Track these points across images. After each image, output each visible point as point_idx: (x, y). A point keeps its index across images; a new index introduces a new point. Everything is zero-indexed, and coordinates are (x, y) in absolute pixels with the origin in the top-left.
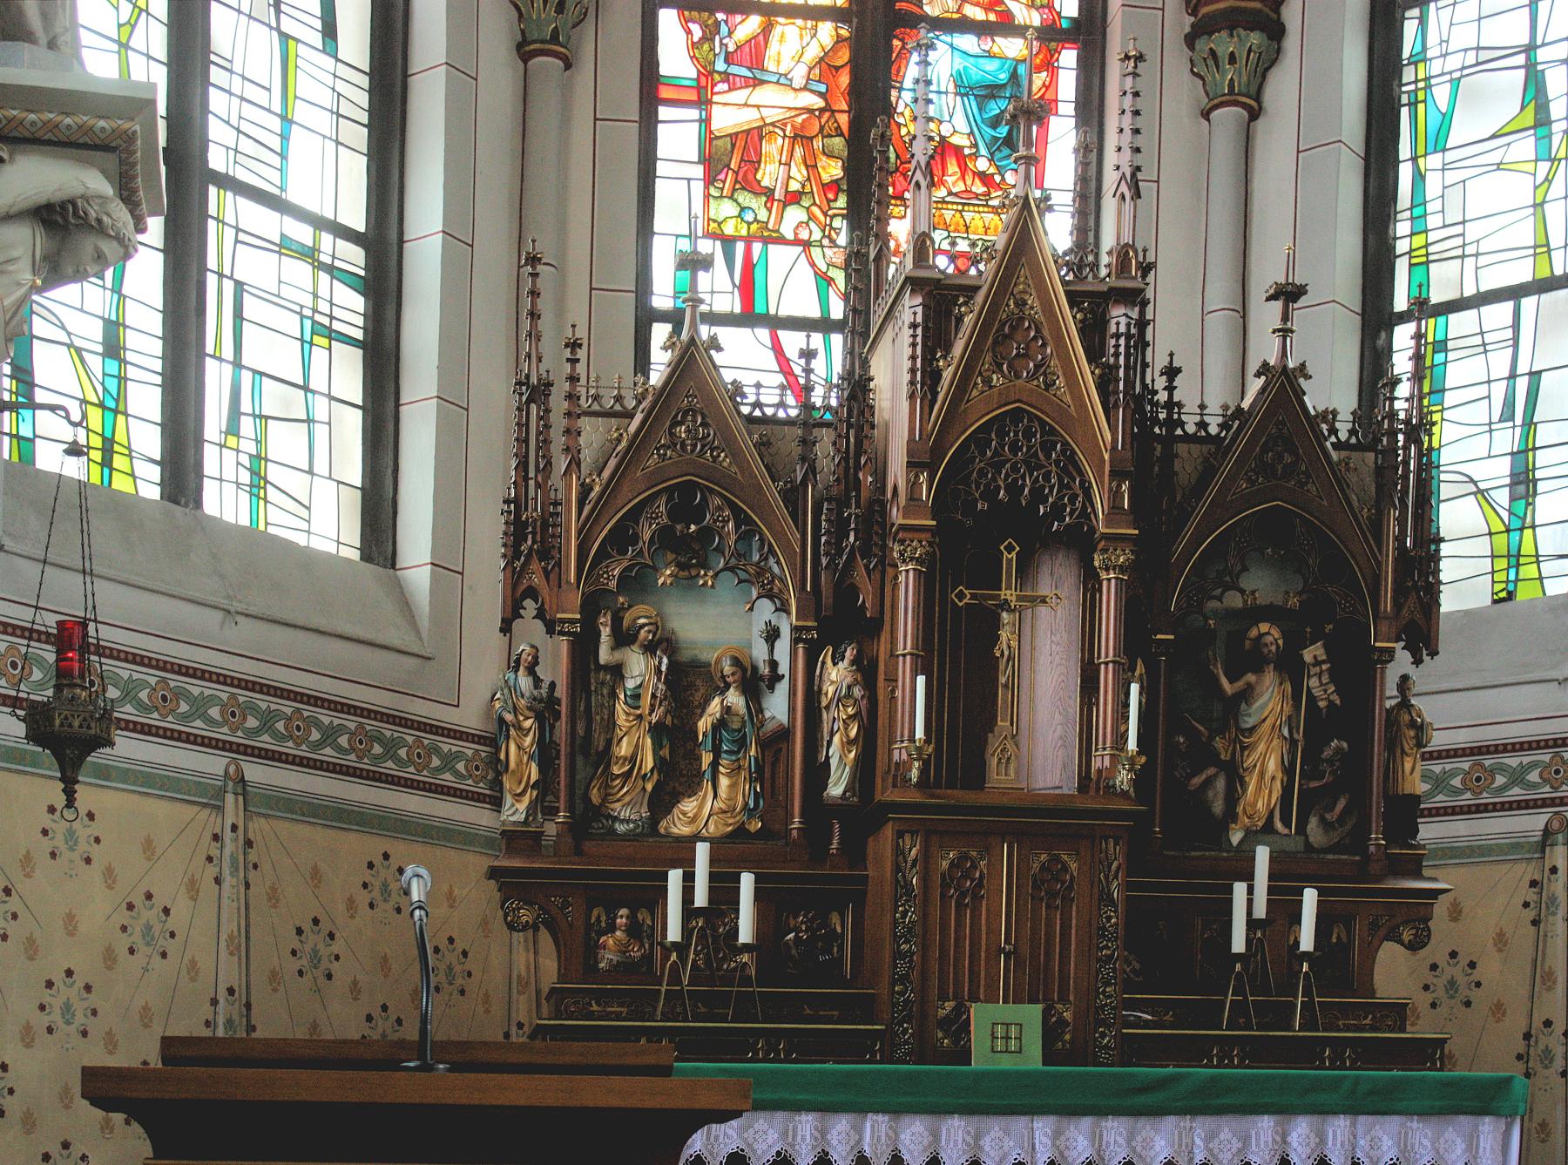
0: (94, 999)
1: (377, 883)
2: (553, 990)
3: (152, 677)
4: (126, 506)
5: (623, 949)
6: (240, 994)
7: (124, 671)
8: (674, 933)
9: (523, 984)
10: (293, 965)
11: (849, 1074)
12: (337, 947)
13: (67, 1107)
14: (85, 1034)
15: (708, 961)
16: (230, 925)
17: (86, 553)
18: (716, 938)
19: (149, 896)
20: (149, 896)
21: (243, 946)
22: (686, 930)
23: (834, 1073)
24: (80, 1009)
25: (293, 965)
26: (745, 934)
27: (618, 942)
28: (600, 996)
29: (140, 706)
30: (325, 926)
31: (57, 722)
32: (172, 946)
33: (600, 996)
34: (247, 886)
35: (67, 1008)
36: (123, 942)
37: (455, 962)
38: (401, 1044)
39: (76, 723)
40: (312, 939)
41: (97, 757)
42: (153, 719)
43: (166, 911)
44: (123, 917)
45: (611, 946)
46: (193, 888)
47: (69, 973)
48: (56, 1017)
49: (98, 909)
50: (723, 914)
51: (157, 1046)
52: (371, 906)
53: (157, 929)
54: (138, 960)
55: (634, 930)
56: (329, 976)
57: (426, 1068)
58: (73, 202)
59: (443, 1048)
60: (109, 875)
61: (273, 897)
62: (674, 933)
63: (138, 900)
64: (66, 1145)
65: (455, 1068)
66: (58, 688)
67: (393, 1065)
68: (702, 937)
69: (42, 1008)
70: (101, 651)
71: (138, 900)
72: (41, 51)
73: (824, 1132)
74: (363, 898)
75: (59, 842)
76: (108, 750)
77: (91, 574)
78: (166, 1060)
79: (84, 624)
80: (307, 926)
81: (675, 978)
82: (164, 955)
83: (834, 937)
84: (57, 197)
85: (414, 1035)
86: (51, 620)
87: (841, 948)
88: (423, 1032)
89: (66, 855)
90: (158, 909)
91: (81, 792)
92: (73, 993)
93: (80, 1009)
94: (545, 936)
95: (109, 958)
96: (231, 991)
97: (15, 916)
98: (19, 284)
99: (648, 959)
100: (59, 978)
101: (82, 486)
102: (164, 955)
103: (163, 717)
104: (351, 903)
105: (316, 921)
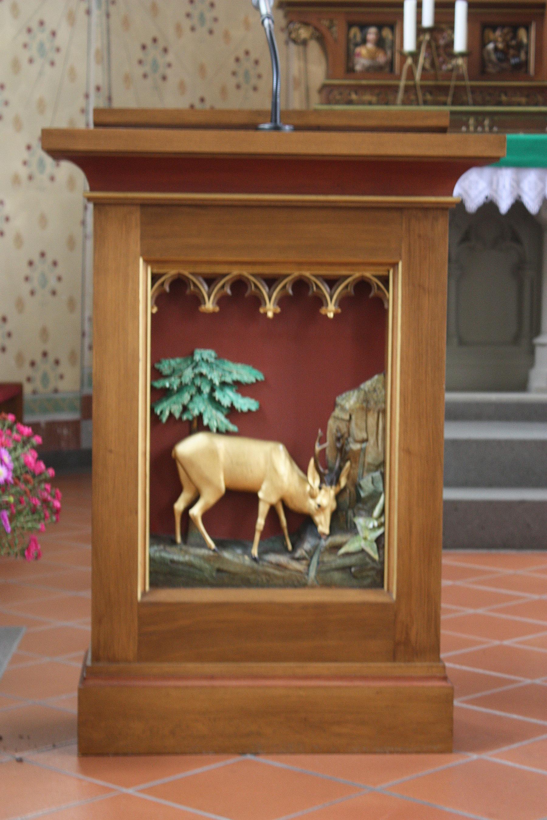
1: (196, 14)
2: (324, 87)
5: (373, 57)
6: (104, 92)
8: (409, 43)
9: (297, 83)
10: (139, 71)
11: (536, 142)
12: (170, 57)
15: (433, 64)
16: (97, 43)
18: (438, 47)
19: (42, 23)
20: (42, 23)
21: (105, 57)
22: (419, 45)
23: (524, 141)
25: (139, 71)
26: (460, 43)
27: (369, 51)
28: (358, 89)
30: (161, 44)
32: (58, 58)
33: (358, 89)
34: (108, 15)
36: (24, 56)
38: (259, 113)
40: (153, 52)
43: (54, 34)
44: (24, 38)
45: (364, 55)
46: (71, 18)
50: (441, 31)
51: (39, 133)
52: (193, 29)
53: (47, 46)
55: (380, 43)
56: (164, 78)
57: (277, 128)
59: (288, 115)
61: (126, 23)
62: (409, 43)
63: (34, 25)
65: (297, 128)
67: (255, 127)
68: (429, 46)
71: (34, 25)
73: (518, 183)
74: (186, 24)
78: (96, 125)
80: (149, 43)
81: (411, 75)
82: (52, 64)
83: (520, 46)
85: (268, 106)
87: (527, 53)
88: (275, 104)
90: (47, 33)
94: (314, 48)
96: (98, 89)
99: (391, 64)
102: (52, 64)
104: (178, 28)
105: (155, 40)
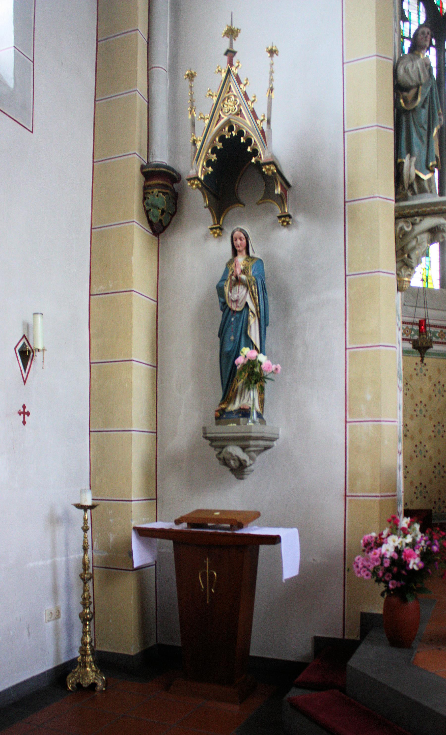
0: (427, 408)
3: (439, 330)
4: (432, 291)
7: (433, 329)
13: (253, 471)
14: (425, 416)
17: (425, 303)
20: (439, 382)
24: (423, 410)
29: (436, 337)
31: (420, 344)
35: (421, 410)
37: (422, 408)
39: (424, 344)
41: (429, 351)
42: (440, 340)
43: (443, 386)
44: (433, 388)
47: (421, 402)
48: (418, 412)
49: (427, 386)
53: (441, 390)
54: (436, 399)
58: (437, 227)
60: (430, 378)
64: (421, 443)
66: (420, 336)
69: (415, 410)
70: (430, 326)
72: (429, 194)
75: (418, 371)
76: (431, 349)
77: (427, 308)
79: (425, 320)
82: (443, 396)
84: (435, 225)
86: (417, 320)
89: (420, 374)
91: (425, 360)
92: (422, 407)
93: (423, 410)
95: (430, 398)
97: (408, 389)
98: (424, 247)
100: (419, 403)
101: (424, 288)
102: (443, 396)
103: (442, 339)
